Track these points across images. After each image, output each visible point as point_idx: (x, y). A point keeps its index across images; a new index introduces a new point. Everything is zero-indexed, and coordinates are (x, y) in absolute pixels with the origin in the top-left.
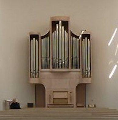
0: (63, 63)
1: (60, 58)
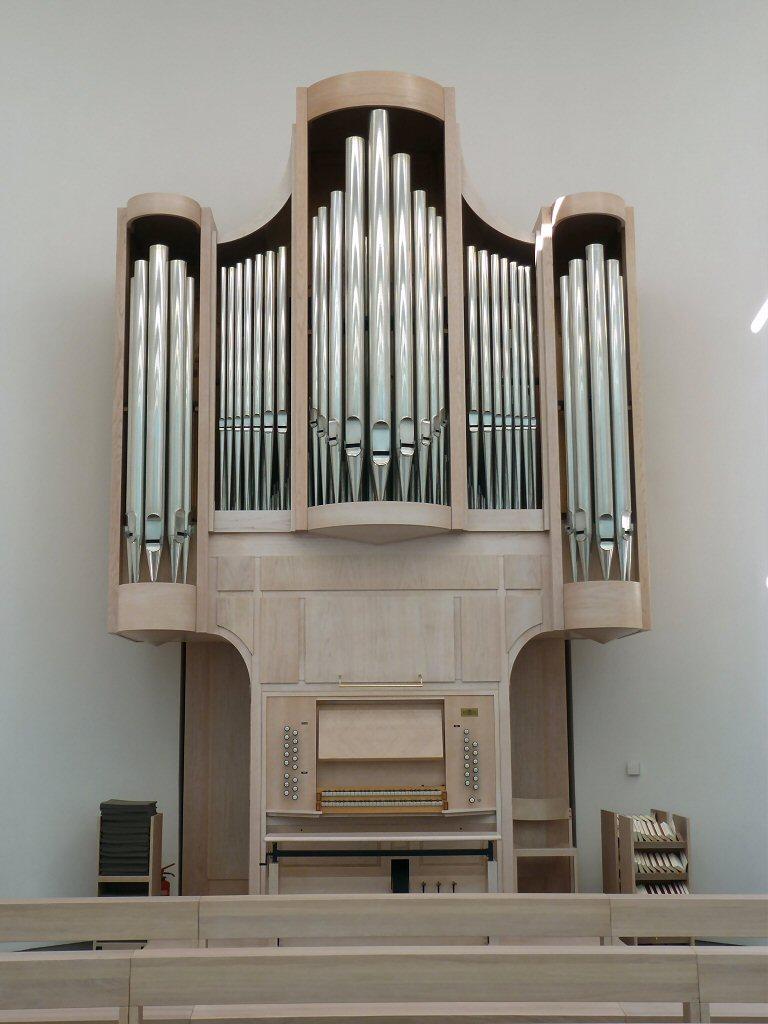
0: (608, 547)
1: (380, 411)
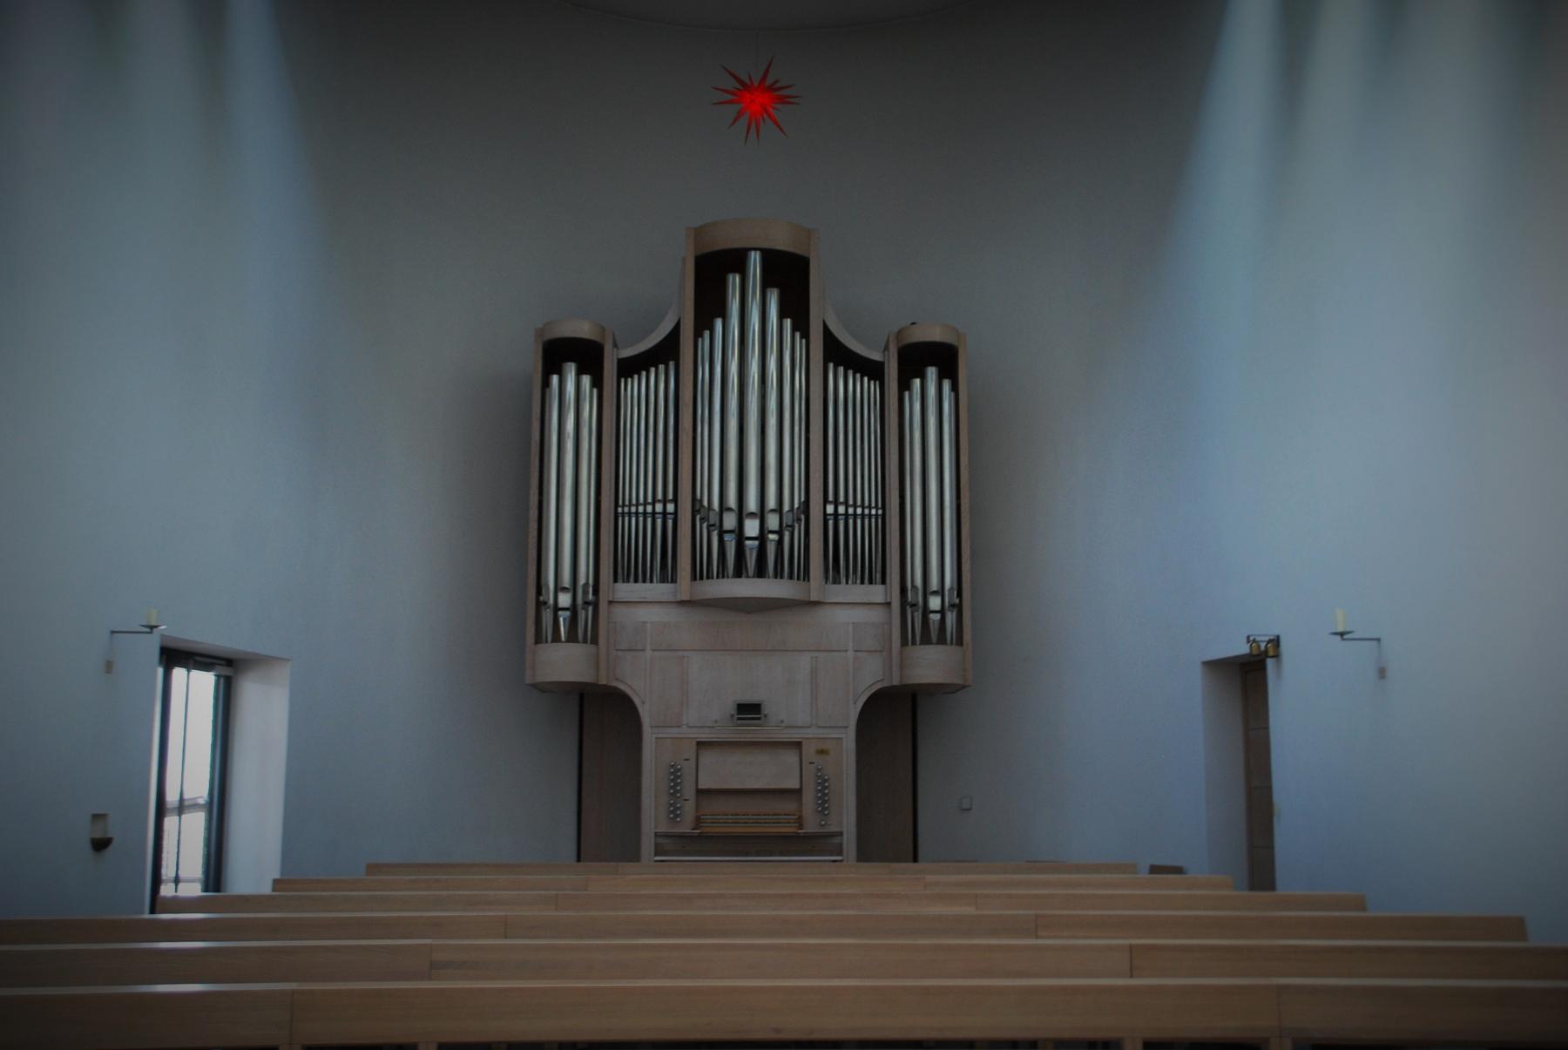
1: (752, 504)
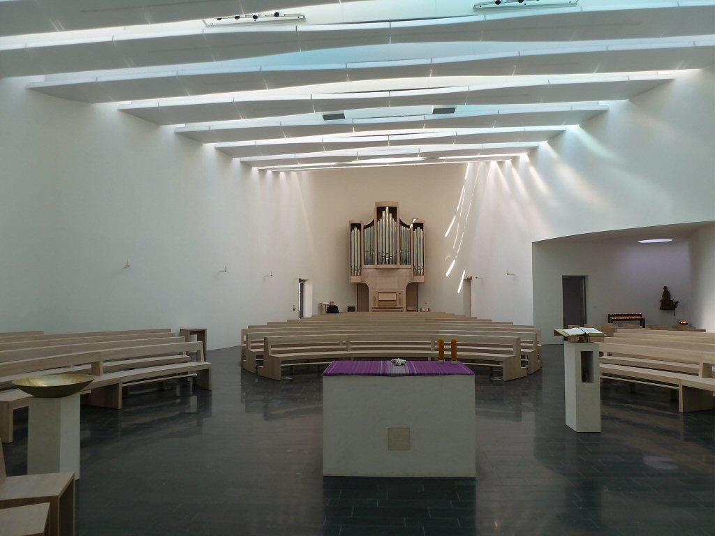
1: (387, 252)
